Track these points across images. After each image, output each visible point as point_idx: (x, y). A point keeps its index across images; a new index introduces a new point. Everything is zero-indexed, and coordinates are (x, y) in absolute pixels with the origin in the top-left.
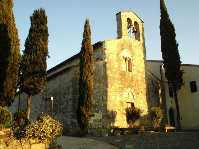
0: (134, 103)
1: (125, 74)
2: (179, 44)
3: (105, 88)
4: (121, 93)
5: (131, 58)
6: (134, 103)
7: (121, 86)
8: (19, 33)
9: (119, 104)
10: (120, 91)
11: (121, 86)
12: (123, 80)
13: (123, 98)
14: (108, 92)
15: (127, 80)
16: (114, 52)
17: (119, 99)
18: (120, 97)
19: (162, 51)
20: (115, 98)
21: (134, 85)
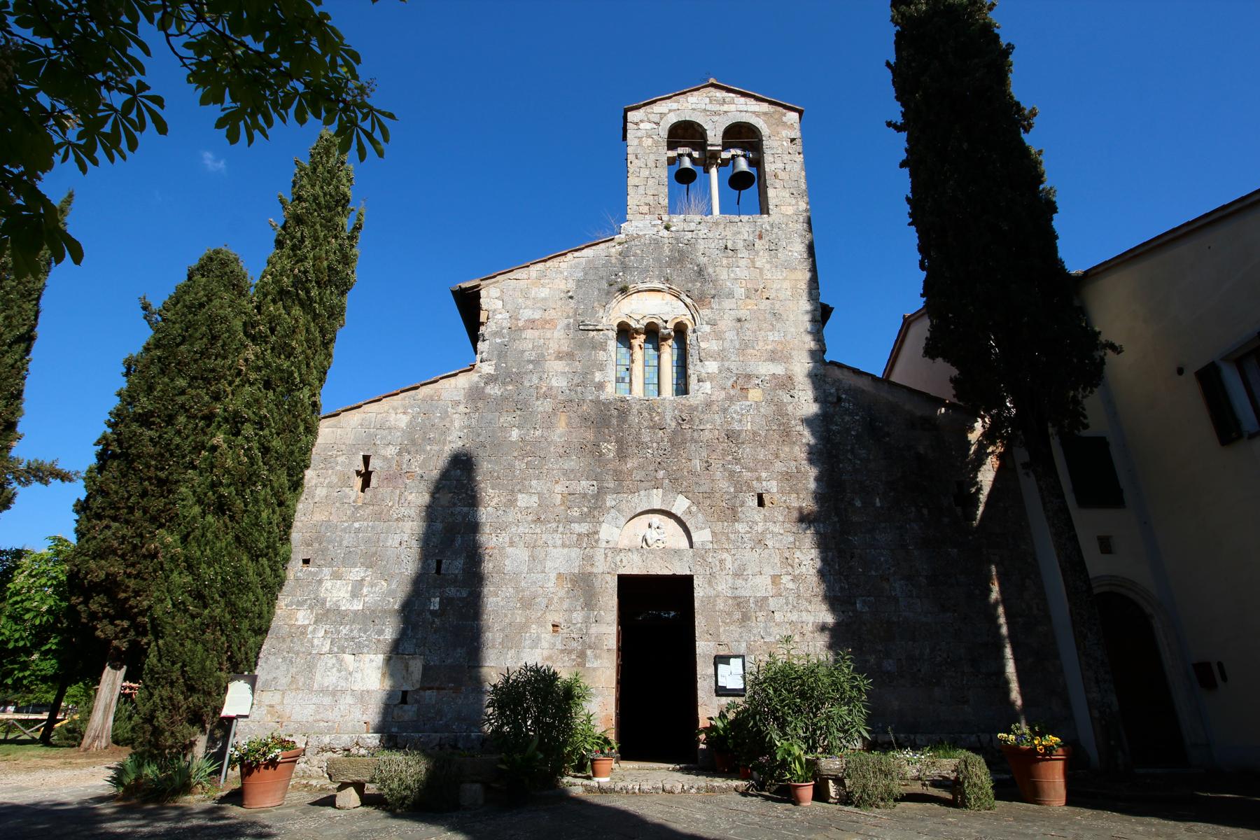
0: (677, 591)
1: (623, 414)
2: (95, 441)
3: (465, 509)
4: (583, 528)
5: (687, 319)
6: (677, 591)
7: (584, 485)
8: (36, 347)
9: (562, 593)
10: (575, 512)
11: (583, 483)
12: (609, 449)
13: (599, 555)
14: (487, 529)
15: (640, 444)
16: (552, 314)
17: (561, 559)
18: (575, 553)
19: (917, 218)
20: (533, 558)
21: (697, 464)
